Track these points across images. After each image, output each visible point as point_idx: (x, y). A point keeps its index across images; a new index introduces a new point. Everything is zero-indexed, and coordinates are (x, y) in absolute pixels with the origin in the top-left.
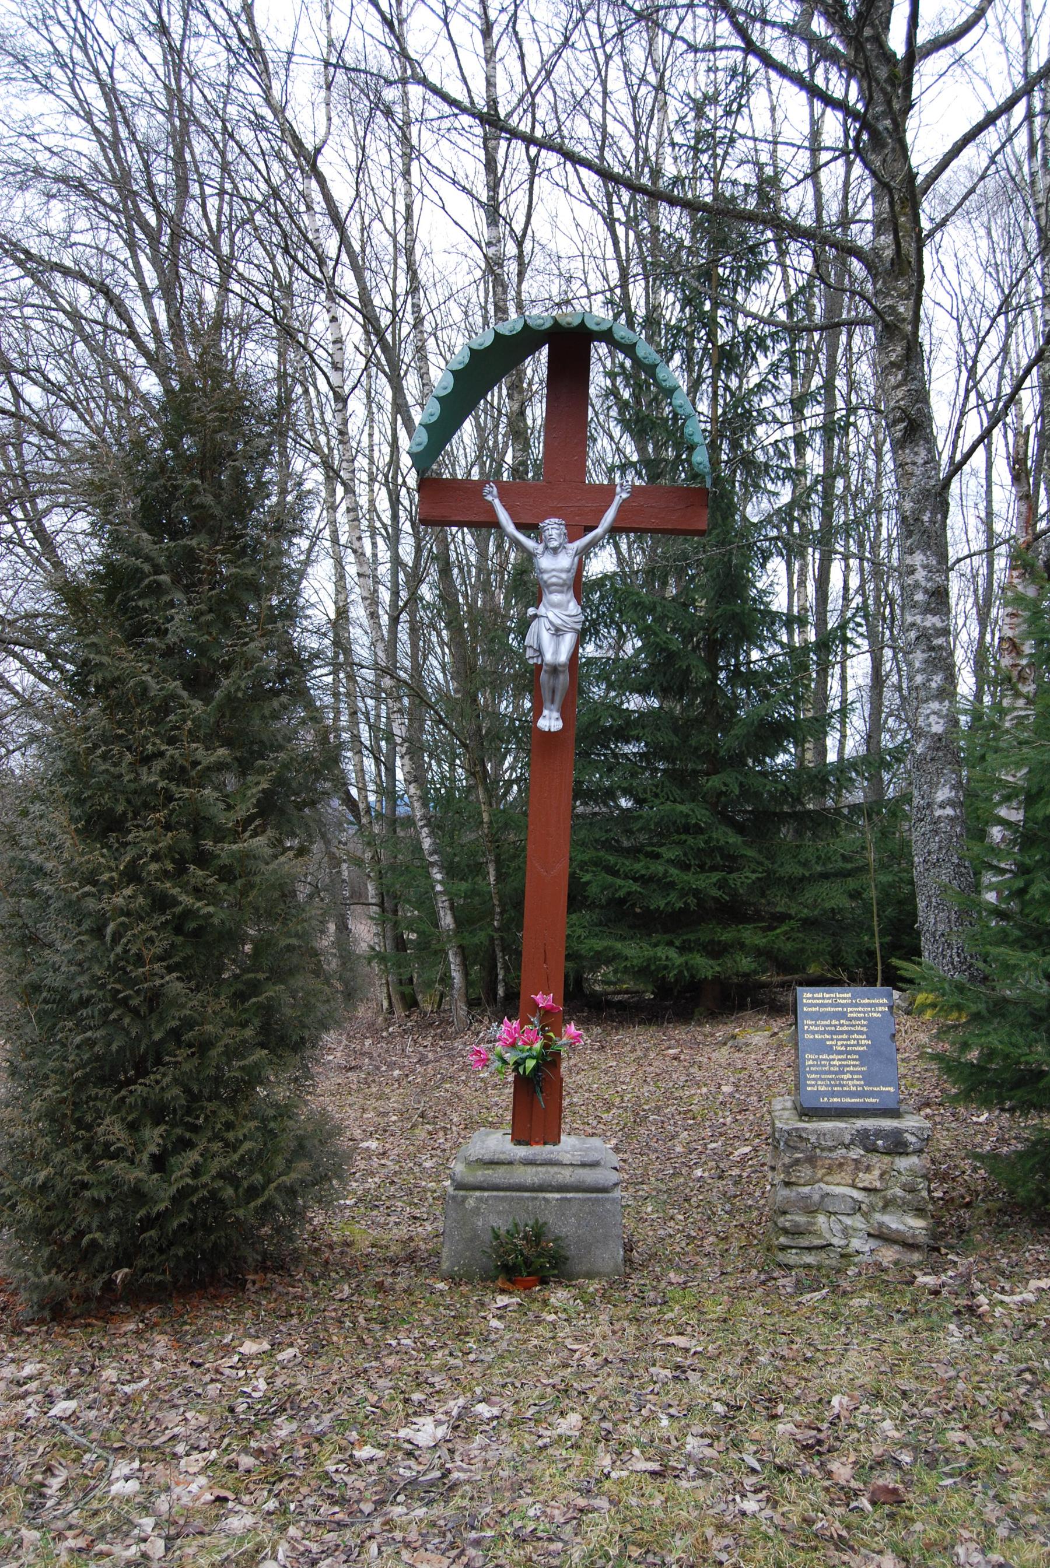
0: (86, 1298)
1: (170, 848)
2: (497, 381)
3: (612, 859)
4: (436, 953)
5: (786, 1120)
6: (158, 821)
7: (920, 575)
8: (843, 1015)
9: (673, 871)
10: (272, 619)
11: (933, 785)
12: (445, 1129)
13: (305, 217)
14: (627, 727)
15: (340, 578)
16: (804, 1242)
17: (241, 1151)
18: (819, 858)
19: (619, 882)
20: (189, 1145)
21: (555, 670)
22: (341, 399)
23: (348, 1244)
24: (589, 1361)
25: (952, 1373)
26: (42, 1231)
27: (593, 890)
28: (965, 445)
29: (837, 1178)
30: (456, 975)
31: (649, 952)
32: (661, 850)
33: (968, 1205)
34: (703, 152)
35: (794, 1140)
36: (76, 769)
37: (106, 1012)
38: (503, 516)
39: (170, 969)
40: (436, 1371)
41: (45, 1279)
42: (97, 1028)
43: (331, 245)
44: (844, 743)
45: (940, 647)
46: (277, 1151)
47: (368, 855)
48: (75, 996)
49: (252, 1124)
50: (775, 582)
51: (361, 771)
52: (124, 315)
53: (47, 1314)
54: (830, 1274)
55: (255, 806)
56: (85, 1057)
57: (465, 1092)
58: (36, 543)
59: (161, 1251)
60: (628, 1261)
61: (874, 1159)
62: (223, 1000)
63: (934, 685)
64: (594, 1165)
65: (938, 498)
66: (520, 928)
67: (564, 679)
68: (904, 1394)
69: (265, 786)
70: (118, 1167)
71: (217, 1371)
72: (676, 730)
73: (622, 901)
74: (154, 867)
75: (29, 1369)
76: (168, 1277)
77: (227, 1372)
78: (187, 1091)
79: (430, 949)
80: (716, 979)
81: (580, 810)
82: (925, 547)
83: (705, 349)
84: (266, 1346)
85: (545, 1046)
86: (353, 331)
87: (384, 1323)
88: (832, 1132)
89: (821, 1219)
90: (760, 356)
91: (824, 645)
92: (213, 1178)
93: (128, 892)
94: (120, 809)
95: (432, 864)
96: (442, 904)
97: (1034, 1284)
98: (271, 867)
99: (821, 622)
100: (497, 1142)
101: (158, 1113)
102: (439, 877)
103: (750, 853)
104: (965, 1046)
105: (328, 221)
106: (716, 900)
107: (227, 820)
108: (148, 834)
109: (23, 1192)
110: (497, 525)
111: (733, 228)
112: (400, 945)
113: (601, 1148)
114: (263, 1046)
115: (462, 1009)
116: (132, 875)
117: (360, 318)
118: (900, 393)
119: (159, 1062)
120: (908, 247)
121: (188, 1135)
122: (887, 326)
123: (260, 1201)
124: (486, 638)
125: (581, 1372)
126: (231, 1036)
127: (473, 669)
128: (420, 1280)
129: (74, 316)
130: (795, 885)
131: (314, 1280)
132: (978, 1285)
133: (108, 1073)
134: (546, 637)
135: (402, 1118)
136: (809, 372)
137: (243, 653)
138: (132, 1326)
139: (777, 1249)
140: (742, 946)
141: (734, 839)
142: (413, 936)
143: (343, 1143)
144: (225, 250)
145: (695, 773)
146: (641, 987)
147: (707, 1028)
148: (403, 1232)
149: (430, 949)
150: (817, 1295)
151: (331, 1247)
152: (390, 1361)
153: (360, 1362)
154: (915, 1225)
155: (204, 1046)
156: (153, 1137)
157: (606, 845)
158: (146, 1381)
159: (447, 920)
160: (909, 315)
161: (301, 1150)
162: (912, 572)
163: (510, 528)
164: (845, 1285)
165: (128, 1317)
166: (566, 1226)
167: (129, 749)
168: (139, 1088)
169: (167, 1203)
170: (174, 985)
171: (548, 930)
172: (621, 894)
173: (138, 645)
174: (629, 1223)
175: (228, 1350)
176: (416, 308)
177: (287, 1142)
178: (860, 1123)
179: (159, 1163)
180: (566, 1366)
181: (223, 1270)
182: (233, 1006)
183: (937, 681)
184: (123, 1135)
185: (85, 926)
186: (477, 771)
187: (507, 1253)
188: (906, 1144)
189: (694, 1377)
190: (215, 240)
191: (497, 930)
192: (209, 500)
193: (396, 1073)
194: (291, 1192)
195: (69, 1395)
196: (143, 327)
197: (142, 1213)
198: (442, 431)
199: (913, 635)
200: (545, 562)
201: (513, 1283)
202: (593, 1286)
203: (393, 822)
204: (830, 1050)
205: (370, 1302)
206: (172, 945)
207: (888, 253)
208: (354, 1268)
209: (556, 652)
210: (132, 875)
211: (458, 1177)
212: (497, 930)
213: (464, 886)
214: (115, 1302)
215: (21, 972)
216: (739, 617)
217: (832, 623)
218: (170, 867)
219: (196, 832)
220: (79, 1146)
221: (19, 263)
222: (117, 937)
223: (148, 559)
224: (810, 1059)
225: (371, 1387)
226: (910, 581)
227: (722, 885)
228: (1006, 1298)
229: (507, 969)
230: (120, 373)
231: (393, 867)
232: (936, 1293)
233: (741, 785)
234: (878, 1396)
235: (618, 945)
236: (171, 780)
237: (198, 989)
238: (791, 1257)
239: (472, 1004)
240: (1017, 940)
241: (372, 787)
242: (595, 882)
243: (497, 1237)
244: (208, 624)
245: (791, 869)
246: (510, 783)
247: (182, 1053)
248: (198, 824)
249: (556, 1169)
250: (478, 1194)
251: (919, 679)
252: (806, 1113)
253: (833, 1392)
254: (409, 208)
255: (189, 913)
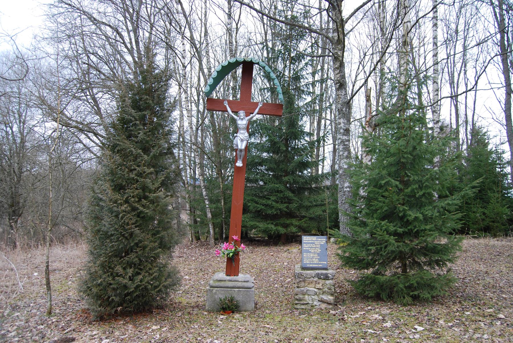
0: (109, 315)
1: (137, 194)
2: (229, 73)
3: (257, 199)
4: (206, 224)
5: (298, 269)
6: (134, 187)
7: (342, 125)
8: (314, 243)
9: (274, 203)
10: (167, 135)
11: (344, 182)
12: (207, 273)
13: (176, 14)
14: (262, 162)
15: (184, 119)
16: (302, 302)
17: (153, 276)
18: (314, 200)
19: (258, 206)
20: (139, 274)
21: (241, 150)
22: (185, 67)
23: (180, 303)
24: (244, 331)
25: (335, 333)
26: (98, 297)
27: (251, 208)
28: (356, 87)
29: (311, 286)
30: (212, 231)
31: (266, 226)
32: (271, 197)
33: (346, 294)
34: (289, 3)
35: (300, 275)
36: (112, 173)
37: (119, 238)
38: (229, 109)
39: (136, 227)
40: (204, 333)
41: (99, 309)
42: (116, 242)
43: (183, 22)
44: (326, 167)
45: (347, 145)
46: (163, 276)
47: (187, 196)
48: (110, 233)
49: (157, 269)
50: (306, 123)
51: (187, 175)
52: (121, 37)
53: (99, 319)
54: (308, 310)
55: (160, 184)
56: (112, 250)
57: (213, 264)
58: (92, 101)
59: (131, 302)
60: (256, 307)
61: (320, 281)
62: (150, 236)
63: (345, 155)
64: (247, 281)
65: (348, 104)
66: (230, 218)
67: (243, 153)
68: (323, 338)
69: (163, 179)
70: (121, 279)
71: (146, 333)
72: (276, 163)
73: (259, 211)
74: (133, 199)
75: (94, 333)
76: (132, 309)
77: (149, 333)
78: (140, 259)
79: (204, 223)
80: (285, 234)
81: (248, 185)
82: (344, 117)
83: (287, 58)
84: (159, 327)
85: (235, 250)
86: (188, 46)
87: (190, 322)
88: (310, 274)
89: (306, 296)
90: (303, 60)
91: (318, 141)
92: (146, 283)
93: (125, 206)
94: (124, 184)
95: (206, 199)
96: (208, 210)
97: (360, 313)
98: (164, 200)
99: (318, 134)
100: (222, 275)
101: (130, 265)
102: (207, 203)
103: (295, 199)
104: (345, 252)
105: (182, 15)
106: (285, 212)
107: (152, 187)
108: (132, 191)
109: (93, 286)
110: (227, 111)
111: (296, 28)
112: (196, 222)
113: (248, 277)
114: (160, 248)
115: (213, 241)
116: (127, 201)
117: (189, 42)
118: (338, 76)
119: (132, 251)
120: (341, 36)
121: (139, 271)
122: (335, 58)
123: (158, 289)
124: (223, 136)
125: (241, 332)
126: (152, 245)
127: (219, 144)
128: (200, 311)
129: (108, 38)
130: (308, 208)
131: (171, 312)
132: (345, 313)
133: (118, 254)
134: (239, 142)
135: (196, 269)
136: (317, 65)
137: (158, 144)
138: (122, 322)
139: (295, 304)
140: (292, 225)
141: (291, 194)
142: (199, 220)
143: (178, 275)
144: (152, 21)
145: (281, 176)
146: (264, 236)
147: (282, 248)
148: (196, 300)
149: (204, 223)
150: (304, 316)
151: (176, 303)
152: (192, 331)
153: (184, 331)
154: (330, 298)
155: (144, 248)
156: (130, 271)
157: (255, 195)
158: (127, 335)
159: (209, 215)
160: (341, 55)
161: (169, 276)
162: (340, 124)
163: (231, 113)
164: (312, 313)
165: (121, 320)
166: (239, 297)
167: (127, 167)
168: (127, 258)
169: (133, 289)
170: (137, 231)
171: (237, 218)
172: (259, 209)
173: (130, 140)
174: (257, 298)
175: (148, 328)
176: (207, 40)
177: (166, 274)
178: (317, 271)
179: (131, 279)
180: (238, 332)
181: (147, 308)
182: (152, 237)
183: (346, 154)
184: (122, 271)
185: (113, 215)
186: (219, 173)
187: (224, 304)
188: (328, 277)
189: (270, 334)
190: (149, 17)
191: (224, 218)
192: (151, 102)
193: (194, 258)
194: (166, 287)
195: (106, 338)
196: (127, 40)
197: (126, 292)
198: (213, 87)
199: (340, 141)
200: (239, 122)
201: (225, 312)
202: (246, 314)
203: (195, 187)
204: (310, 252)
205: (186, 317)
206: (137, 220)
207: (336, 38)
208: (182, 309)
209: (241, 146)
210: (127, 201)
211: (211, 284)
212: (224, 218)
213: (214, 206)
214: (117, 316)
215: (95, 226)
216: (295, 132)
217: (321, 134)
218: (137, 200)
219: (143, 190)
220: (109, 274)
221: (92, 21)
222: (122, 218)
223: (133, 117)
224: (305, 254)
225: (187, 336)
226: (339, 126)
227: (287, 207)
228: (352, 316)
229: (226, 230)
230: (120, 54)
231: (194, 200)
232: (335, 315)
233: (293, 180)
234: (316, 338)
235: (258, 224)
236: (138, 176)
237: (143, 232)
238: (298, 306)
239: (216, 239)
240: (359, 225)
241: (188, 176)
242: (252, 206)
243: (221, 300)
244: (149, 135)
245: (307, 203)
246: (228, 176)
247: (138, 250)
248: (144, 188)
249: (237, 283)
250: (216, 289)
251: (341, 153)
252: (304, 268)
253: (305, 337)
254: (206, 12)
255: (141, 212)
